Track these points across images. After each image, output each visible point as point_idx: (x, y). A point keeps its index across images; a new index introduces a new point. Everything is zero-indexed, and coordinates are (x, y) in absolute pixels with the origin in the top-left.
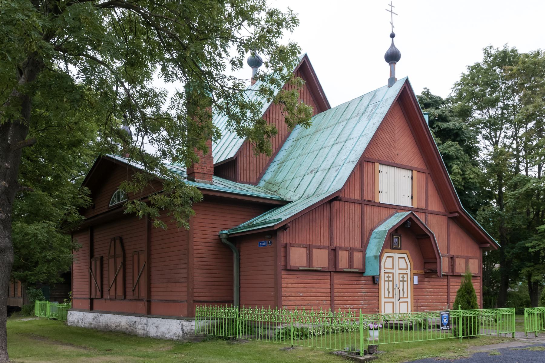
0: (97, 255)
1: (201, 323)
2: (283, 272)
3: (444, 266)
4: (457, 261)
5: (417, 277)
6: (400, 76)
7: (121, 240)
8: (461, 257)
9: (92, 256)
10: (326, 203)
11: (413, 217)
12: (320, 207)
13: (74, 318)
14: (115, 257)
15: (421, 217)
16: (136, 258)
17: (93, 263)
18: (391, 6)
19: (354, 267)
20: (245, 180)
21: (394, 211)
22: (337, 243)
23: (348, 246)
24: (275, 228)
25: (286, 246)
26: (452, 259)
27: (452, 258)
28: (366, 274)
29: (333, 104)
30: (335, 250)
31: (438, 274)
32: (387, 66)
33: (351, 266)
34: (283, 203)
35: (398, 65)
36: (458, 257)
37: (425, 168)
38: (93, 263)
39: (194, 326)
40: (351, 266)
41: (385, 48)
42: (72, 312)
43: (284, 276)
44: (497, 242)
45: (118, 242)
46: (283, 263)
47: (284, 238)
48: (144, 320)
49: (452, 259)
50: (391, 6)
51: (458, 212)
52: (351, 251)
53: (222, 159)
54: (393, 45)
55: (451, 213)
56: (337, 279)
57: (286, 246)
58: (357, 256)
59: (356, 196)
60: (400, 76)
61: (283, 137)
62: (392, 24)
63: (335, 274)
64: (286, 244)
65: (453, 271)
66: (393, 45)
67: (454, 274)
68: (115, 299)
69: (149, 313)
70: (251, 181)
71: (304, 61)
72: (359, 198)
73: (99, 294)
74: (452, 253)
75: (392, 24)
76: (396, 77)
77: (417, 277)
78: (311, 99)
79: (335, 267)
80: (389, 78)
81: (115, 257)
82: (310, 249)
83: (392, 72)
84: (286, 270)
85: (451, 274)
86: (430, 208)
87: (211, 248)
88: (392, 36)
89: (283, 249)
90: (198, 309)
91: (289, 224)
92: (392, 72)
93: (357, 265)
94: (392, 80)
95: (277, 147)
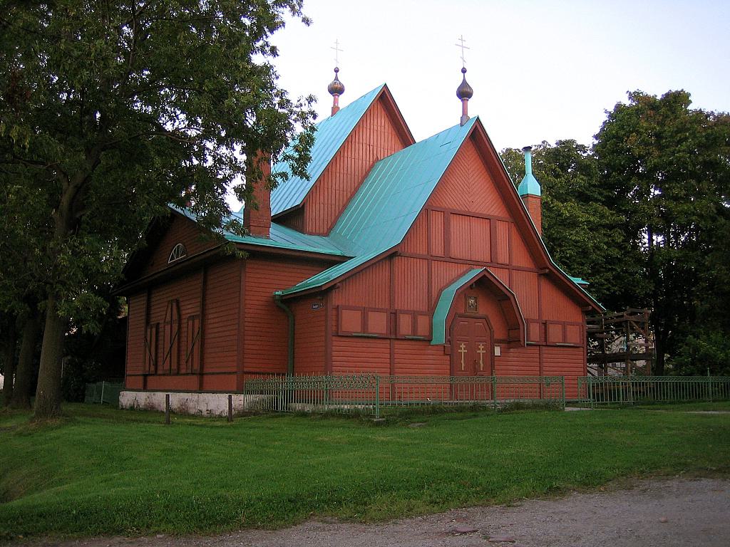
0: (153, 321)
1: (252, 397)
2: (334, 338)
3: (535, 332)
5: (499, 348)
6: (472, 114)
7: (177, 302)
8: (557, 323)
9: (148, 322)
10: (385, 258)
11: (487, 274)
12: (371, 268)
13: (126, 400)
14: (171, 323)
16: (191, 322)
17: (149, 330)
19: (419, 334)
20: (314, 231)
21: (465, 268)
22: (398, 306)
24: (323, 288)
27: (545, 324)
28: (433, 343)
29: (417, 142)
30: (395, 314)
31: (522, 343)
33: (564, 340)
34: (343, 259)
35: (470, 102)
37: (507, 216)
38: (149, 330)
39: (239, 401)
40: (564, 340)
42: (125, 393)
43: (335, 343)
44: (600, 304)
45: (174, 304)
46: (334, 328)
47: (336, 299)
48: (195, 396)
51: (548, 268)
52: (414, 315)
55: (541, 269)
58: (422, 321)
59: (422, 250)
61: (360, 178)
62: (463, 59)
63: (396, 342)
64: (338, 306)
67: (548, 344)
68: (169, 373)
69: (201, 389)
70: (321, 231)
72: (425, 253)
73: (153, 368)
74: (544, 319)
75: (463, 59)
77: (499, 348)
78: (394, 133)
81: (171, 323)
82: (365, 313)
83: (335, 102)
85: (544, 344)
86: (515, 264)
89: (334, 312)
90: (249, 380)
93: (422, 331)
95: (353, 190)
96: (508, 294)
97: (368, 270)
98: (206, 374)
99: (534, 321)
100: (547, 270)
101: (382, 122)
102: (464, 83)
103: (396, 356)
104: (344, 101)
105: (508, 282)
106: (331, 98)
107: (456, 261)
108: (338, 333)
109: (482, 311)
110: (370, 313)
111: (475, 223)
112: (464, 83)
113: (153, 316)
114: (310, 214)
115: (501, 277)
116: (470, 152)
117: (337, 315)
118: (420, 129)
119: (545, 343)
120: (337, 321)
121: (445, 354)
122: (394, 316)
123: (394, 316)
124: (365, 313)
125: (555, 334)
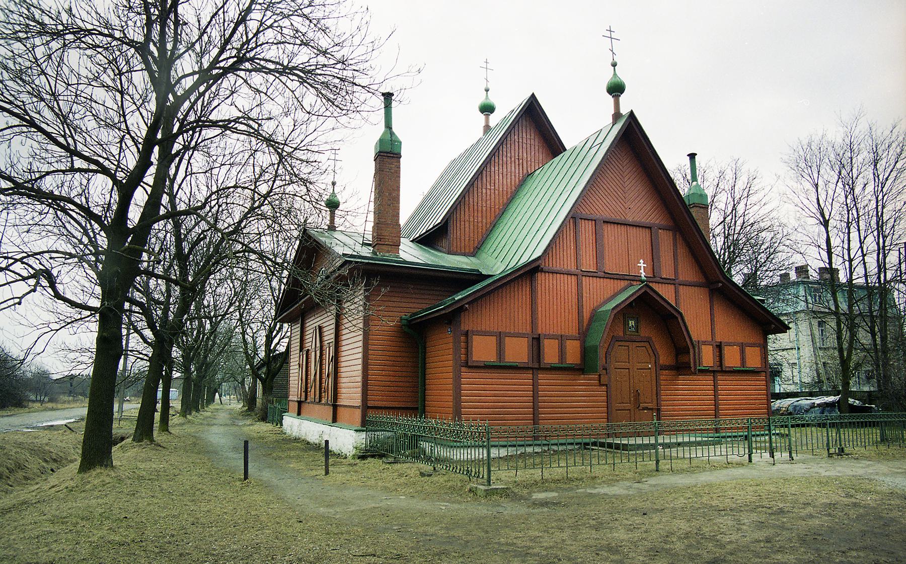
2: (463, 369)
3: (708, 357)
4: (727, 350)
6: (624, 111)
11: (649, 291)
15: (655, 286)
18: (610, 31)
21: (623, 284)
22: (541, 329)
23: (830, 430)
25: (466, 334)
26: (719, 347)
29: (567, 148)
31: (692, 369)
32: (610, 99)
35: (622, 98)
36: (729, 344)
41: (606, 78)
47: (468, 323)
49: (719, 347)
50: (610, 31)
51: (721, 282)
53: (524, 260)
54: (615, 74)
56: (544, 379)
57: (466, 334)
60: (624, 111)
65: (721, 365)
66: (615, 74)
70: (467, 251)
71: (532, 102)
75: (612, 51)
76: (621, 112)
79: (539, 362)
80: (613, 112)
82: (500, 337)
83: (487, 120)
84: (467, 365)
85: (719, 369)
87: (388, 353)
88: (614, 65)
91: (467, 306)
92: (487, 120)
94: (617, 116)
96: (675, 314)
97: (508, 287)
98: (341, 406)
99: (705, 343)
100: (720, 285)
101: (528, 138)
102: (616, 98)
103: (458, 450)
104: (495, 119)
105: (674, 299)
106: (482, 117)
107: (612, 276)
108: (467, 363)
109: (645, 332)
110: (507, 338)
111: (633, 231)
112: (616, 98)
113: (344, 343)
114: (456, 233)
115: (666, 292)
116: (625, 163)
117: (467, 342)
118: (569, 136)
119: (720, 370)
120: (467, 348)
121: (601, 385)
122: (536, 342)
123: (536, 342)
124: (500, 337)
125: (732, 359)
